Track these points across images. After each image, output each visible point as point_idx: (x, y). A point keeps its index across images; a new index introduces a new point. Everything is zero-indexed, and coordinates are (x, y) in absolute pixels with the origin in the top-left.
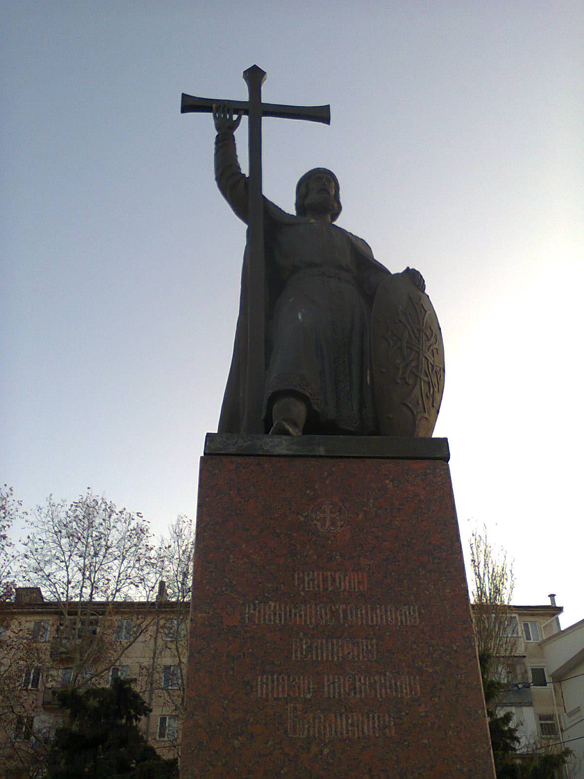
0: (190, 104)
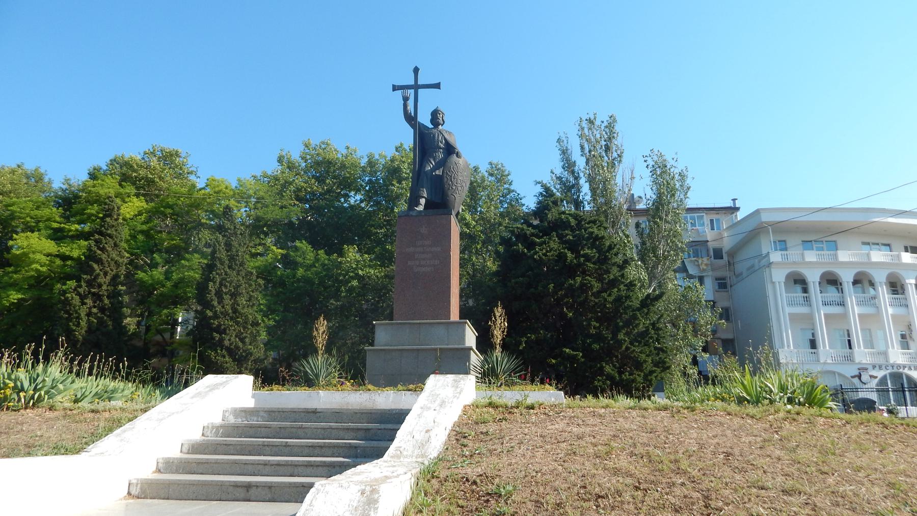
0: (395, 88)
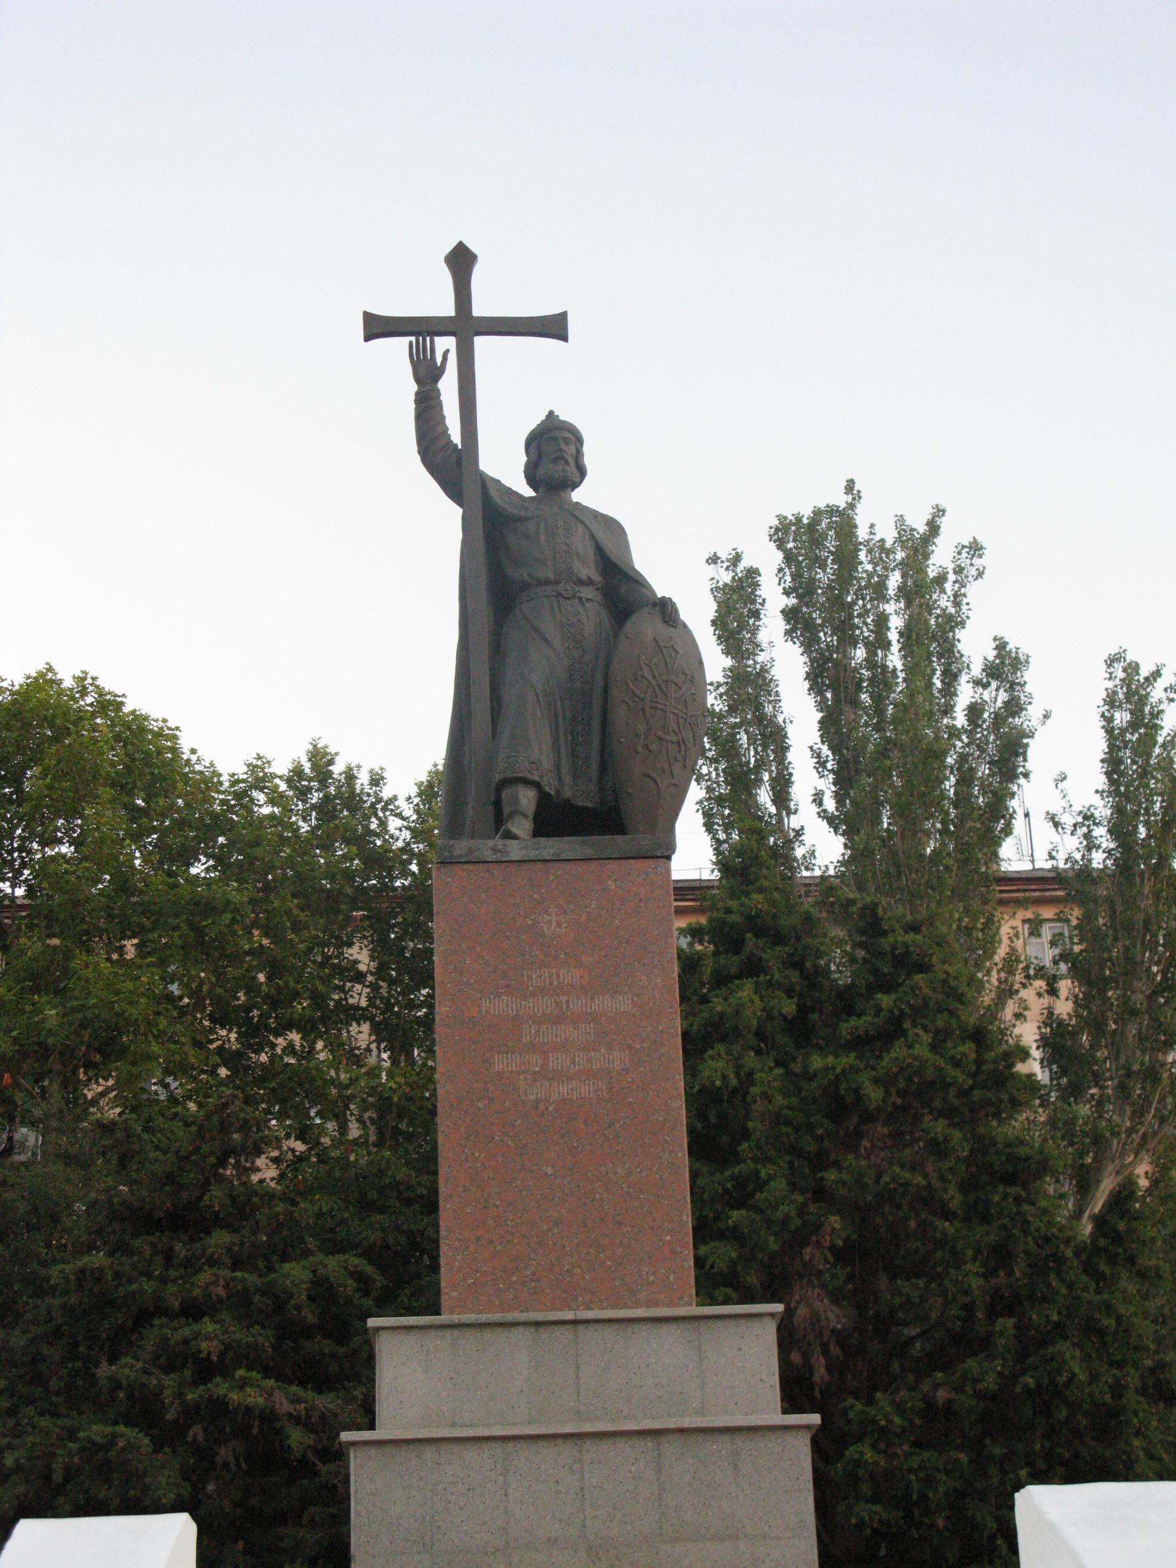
0: (377, 327)
